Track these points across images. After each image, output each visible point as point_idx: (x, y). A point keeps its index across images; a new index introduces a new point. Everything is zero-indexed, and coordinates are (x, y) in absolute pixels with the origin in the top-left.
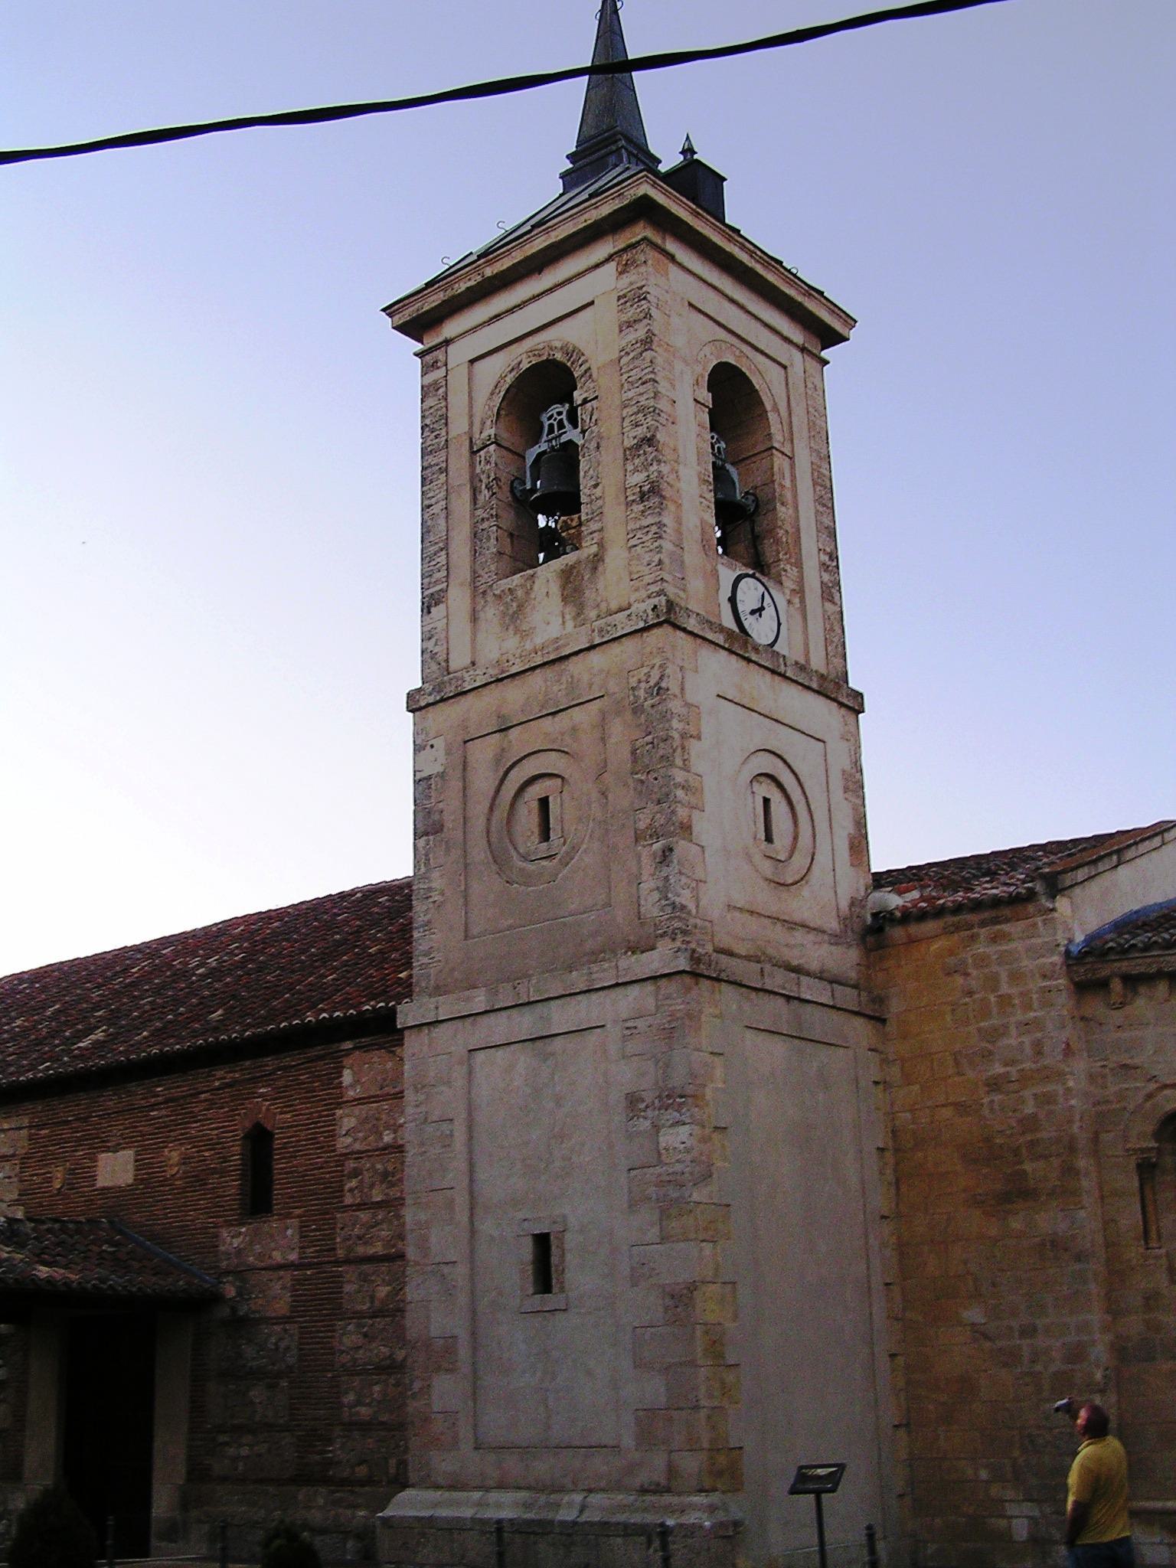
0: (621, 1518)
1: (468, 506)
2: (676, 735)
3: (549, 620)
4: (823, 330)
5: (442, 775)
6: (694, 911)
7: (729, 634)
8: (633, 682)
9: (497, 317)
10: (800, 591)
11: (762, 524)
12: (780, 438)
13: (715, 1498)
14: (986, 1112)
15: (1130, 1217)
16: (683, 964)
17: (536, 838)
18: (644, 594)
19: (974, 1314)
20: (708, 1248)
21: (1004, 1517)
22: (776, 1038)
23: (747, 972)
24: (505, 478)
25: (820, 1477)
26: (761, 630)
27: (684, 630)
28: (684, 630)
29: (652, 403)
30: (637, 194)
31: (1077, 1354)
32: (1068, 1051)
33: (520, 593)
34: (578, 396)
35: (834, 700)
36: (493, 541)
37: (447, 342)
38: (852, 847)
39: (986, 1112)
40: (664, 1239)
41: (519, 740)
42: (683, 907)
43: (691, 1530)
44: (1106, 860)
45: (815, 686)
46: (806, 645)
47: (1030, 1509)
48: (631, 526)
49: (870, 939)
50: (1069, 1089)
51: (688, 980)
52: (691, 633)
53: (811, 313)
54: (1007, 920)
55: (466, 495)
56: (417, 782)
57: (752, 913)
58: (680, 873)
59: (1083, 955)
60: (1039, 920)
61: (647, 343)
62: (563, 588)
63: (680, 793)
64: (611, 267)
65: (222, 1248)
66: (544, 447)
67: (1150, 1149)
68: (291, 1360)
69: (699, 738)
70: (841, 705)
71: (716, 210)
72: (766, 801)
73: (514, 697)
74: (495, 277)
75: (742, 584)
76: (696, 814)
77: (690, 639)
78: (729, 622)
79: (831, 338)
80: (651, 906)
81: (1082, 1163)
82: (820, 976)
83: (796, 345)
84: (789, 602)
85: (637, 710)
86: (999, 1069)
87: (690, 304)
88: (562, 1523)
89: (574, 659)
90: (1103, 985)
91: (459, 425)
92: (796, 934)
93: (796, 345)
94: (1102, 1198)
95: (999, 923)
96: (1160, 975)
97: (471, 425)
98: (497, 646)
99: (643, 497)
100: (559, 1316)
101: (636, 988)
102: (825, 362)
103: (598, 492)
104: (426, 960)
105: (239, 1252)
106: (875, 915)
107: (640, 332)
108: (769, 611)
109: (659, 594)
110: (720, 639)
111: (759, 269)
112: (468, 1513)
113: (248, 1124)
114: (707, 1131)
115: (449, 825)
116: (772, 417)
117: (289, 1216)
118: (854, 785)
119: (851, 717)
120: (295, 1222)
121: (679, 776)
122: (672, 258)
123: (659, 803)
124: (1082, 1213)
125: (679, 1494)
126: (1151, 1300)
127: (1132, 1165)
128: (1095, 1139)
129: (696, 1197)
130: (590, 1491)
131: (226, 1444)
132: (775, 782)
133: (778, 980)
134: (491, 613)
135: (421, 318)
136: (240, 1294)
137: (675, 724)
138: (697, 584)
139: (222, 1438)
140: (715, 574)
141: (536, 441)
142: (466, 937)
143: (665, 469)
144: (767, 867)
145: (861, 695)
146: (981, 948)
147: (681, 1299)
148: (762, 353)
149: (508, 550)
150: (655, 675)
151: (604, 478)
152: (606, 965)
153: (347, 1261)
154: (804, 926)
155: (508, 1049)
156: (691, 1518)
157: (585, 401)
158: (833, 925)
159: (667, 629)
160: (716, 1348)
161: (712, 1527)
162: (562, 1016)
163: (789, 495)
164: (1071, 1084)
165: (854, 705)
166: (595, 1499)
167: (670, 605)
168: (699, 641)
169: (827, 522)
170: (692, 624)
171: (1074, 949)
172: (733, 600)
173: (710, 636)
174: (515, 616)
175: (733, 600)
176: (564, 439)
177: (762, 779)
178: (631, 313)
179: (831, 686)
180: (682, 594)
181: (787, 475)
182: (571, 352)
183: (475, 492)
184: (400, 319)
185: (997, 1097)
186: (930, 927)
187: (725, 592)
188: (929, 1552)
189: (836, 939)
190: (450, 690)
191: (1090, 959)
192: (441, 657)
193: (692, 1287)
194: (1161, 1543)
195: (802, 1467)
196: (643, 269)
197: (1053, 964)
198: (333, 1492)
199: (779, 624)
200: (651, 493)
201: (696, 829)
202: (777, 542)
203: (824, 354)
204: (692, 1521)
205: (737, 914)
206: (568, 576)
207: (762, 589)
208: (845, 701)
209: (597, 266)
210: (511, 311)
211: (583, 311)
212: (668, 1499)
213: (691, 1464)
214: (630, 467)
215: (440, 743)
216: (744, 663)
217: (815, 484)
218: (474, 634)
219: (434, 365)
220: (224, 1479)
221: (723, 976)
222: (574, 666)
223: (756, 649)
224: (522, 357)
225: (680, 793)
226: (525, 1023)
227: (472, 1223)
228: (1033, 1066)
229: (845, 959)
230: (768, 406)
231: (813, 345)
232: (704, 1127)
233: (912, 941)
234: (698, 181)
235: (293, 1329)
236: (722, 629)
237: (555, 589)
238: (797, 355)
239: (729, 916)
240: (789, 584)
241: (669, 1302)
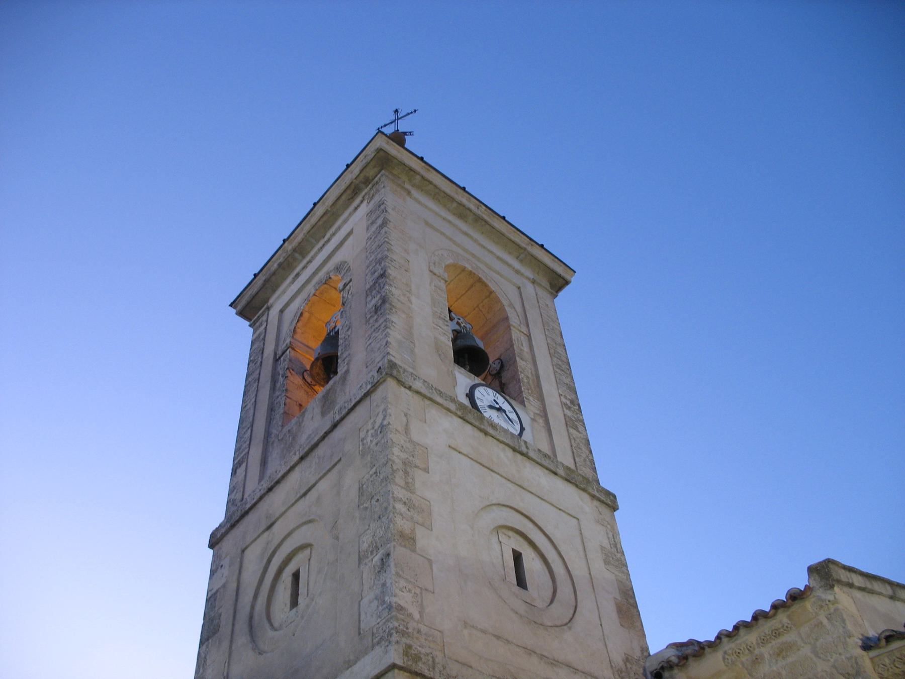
6: (417, 616)
7: (461, 406)
38: (620, 610)
42: (400, 608)
52: (418, 392)
54: (787, 629)
63: (399, 506)
64: (365, 202)
69: (426, 470)
70: (593, 497)
72: (517, 557)
79: (558, 283)
84: (533, 420)
110: (453, 407)
119: (606, 511)
121: (400, 493)
137: (396, 450)
145: (614, 496)
154: (569, 666)
168: (428, 402)
170: (418, 385)
179: (580, 479)
184: (239, 307)
216: (482, 435)
225: (399, 506)
230: (505, 303)
236: (453, 400)
239: (466, 632)
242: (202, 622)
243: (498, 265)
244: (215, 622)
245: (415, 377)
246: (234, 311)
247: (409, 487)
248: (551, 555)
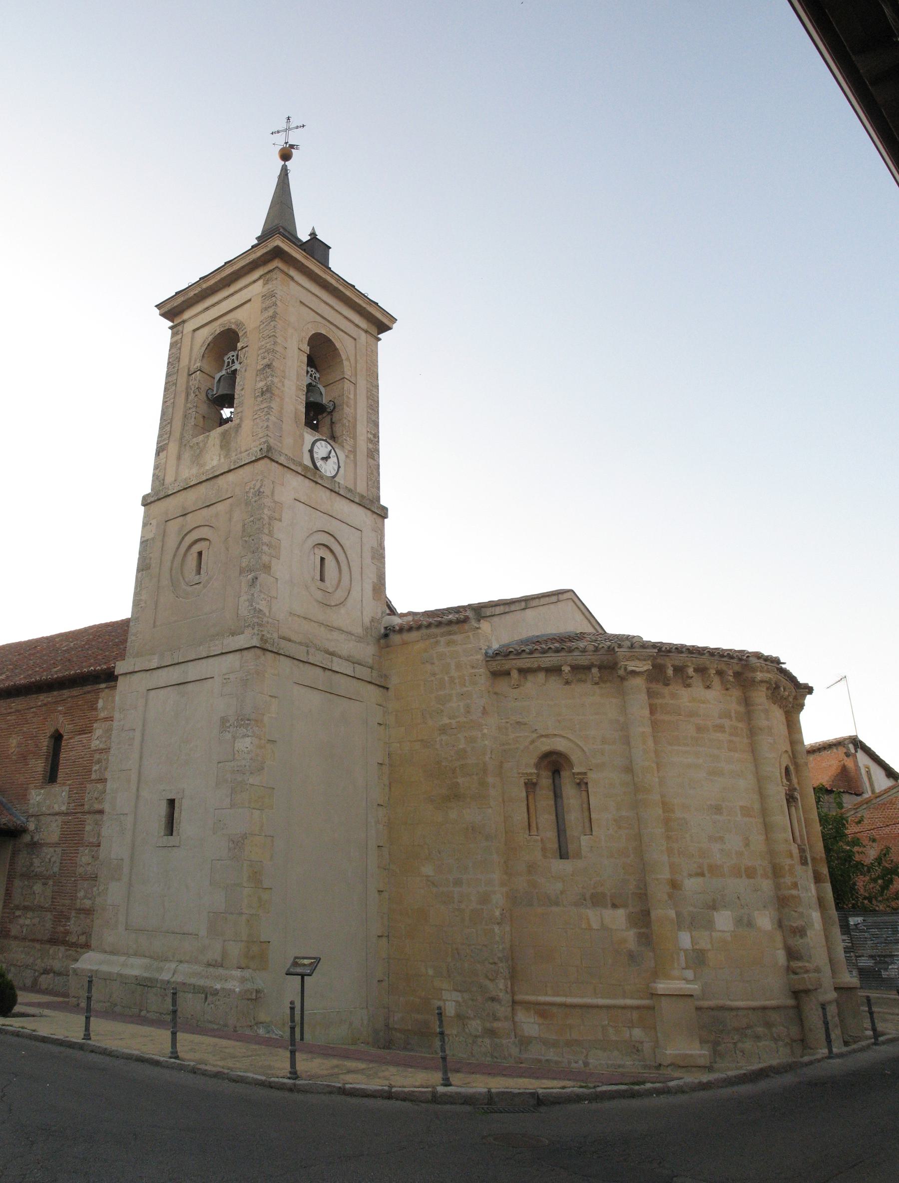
0: (193, 981)
1: (183, 401)
2: (266, 518)
3: (214, 460)
4: (380, 323)
5: (153, 539)
7: (306, 467)
8: (247, 488)
9: (207, 309)
10: (354, 451)
11: (336, 416)
12: (349, 373)
13: (247, 973)
14: (438, 746)
15: (520, 815)
16: (255, 642)
17: (194, 573)
18: (258, 443)
19: (428, 870)
20: (257, 813)
21: (440, 999)
22: (315, 692)
23: (292, 649)
24: (204, 388)
25: (305, 965)
26: (328, 469)
27: (277, 462)
28: (277, 462)
29: (272, 347)
30: (286, 251)
31: (485, 899)
32: (485, 712)
33: (201, 445)
34: (239, 345)
35: (369, 509)
36: (193, 419)
37: (184, 322)
39: (438, 746)
40: (232, 806)
41: (191, 521)
43: (229, 993)
44: (517, 604)
45: (357, 500)
46: (355, 479)
47: (456, 996)
48: (256, 408)
49: (382, 641)
50: (484, 735)
51: (258, 652)
53: (370, 313)
54: (455, 633)
55: (183, 396)
56: (142, 543)
57: (305, 618)
58: (261, 591)
59: (497, 654)
60: (470, 634)
61: (273, 317)
62: (221, 442)
63: (265, 548)
64: (260, 282)
65: (31, 801)
66: (224, 372)
67: (531, 774)
68: (56, 869)
69: (280, 520)
70: (374, 512)
71: (324, 261)
73: (190, 498)
74: (207, 288)
75: (318, 444)
76: (274, 561)
77: (280, 467)
78: (307, 461)
79: (383, 328)
80: (244, 611)
81: (490, 780)
82: (348, 659)
83: (363, 330)
84: (347, 456)
85: (247, 504)
86: (446, 721)
87: (301, 302)
88: (162, 981)
89: (221, 477)
90: (507, 673)
91: (184, 362)
92: (333, 633)
93: (363, 330)
94: (504, 801)
95: (450, 634)
96: (539, 669)
97: (190, 362)
98: (189, 473)
99: (263, 394)
100: (175, 849)
101: (231, 656)
102: (380, 339)
103: (243, 392)
104: (134, 638)
105: (39, 804)
106: (386, 628)
107: (270, 312)
108: (333, 459)
109: (265, 443)
110: (299, 470)
111: (341, 288)
112: (115, 969)
113: (52, 730)
114: (263, 742)
115: (153, 565)
116: (346, 363)
117: (64, 784)
118: (379, 555)
119: (379, 520)
120: (67, 788)
121: (266, 539)
122: (292, 278)
123: (253, 552)
124: (490, 810)
125: (227, 968)
126: (531, 868)
127: (522, 781)
128: (501, 766)
129: (251, 781)
130: (181, 962)
131: (20, 916)
132: (327, 550)
133: (317, 658)
134: (187, 455)
135: (173, 310)
136: (36, 829)
137: (266, 511)
138: (288, 441)
139: (18, 913)
140: (302, 437)
141: (221, 370)
142: (154, 627)
143: (276, 380)
144: (319, 595)
145: (387, 509)
146: (441, 649)
147: (238, 843)
148: (342, 331)
149: (201, 424)
150: (258, 485)
151: (247, 385)
152: (217, 642)
153: (89, 813)
155: (166, 690)
156: (229, 985)
157: (243, 348)
158: (359, 631)
159: (267, 461)
160: (256, 877)
161: (240, 992)
162: (193, 671)
163: (352, 402)
164: (485, 731)
165: (382, 513)
166: (183, 967)
167: (269, 448)
168: (286, 469)
169: (374, 418)
170: (282, 460)
171: (490, 652)
172: (311, 451)
173: (293, 467)
174: (198, 458)
177: (321, 547)
178: (268, 303)
179: (368, 502)
180: (279, 444)
181: (352, 392)
182: (240, 324)
183: (187, 395)
185: (444, 738)
186: (414, 635)
187: (307, 446)
188: (396, 1019)
189: (360, 639)
190: (162, 495)
191: (499, 658)
192: (161, 477)
193: (244, 837)
194: (534, 1023)
195: (296, 958)
196: (275, 282)
197: (478, 660)
198: (67, 950)
199: (339, 467)
200: (267, 392)
201: (272, 570)
202: (343, 425)
203: (380, 336)
204: (229, 987)
205: (296, 618)
206: (224, 435)
207: (329, 448)
208: (376, 511)
210: (213, 305)
211: (245, 305)
212: (221, 971)
213: (235, 950)
215: (154, 522)
216: (313, 484)
217: (368, 398)
218: (178, 466)
220: (16, 938)
221: (281, 652)
222: (221, 481)
223: (322, 477)
224: (217, 328)
225: (265, 548)
226: (174, 675)
227: (138, 790)
228: (465, 720)
229: (367, 651)
230: (344, 357)
231: (373, 330)
232: (260, 739)
233: (405, 643)
234: (317, 248)
235: (59, 850)
236: (301, 464)
237: (218, 442)
238: (363, 335)
239: (290, 619)
240: (348, 447)
241: (231, 845)
242: (138, 556)
243: (344, 324)
244: (148, 561)
245: (280, 453)
246: (158, 311)
247: (270, 534)
248: (341, 557)
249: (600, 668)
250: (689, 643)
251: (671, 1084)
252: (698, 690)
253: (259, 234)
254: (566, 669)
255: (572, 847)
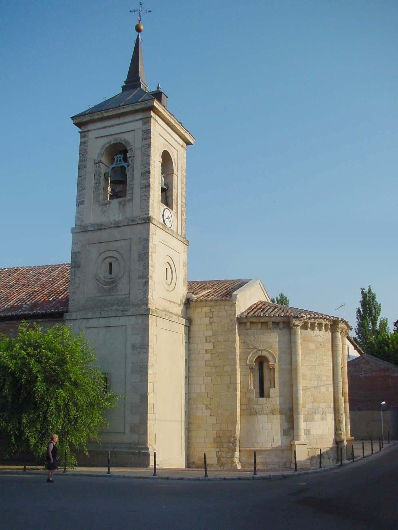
37: (89, 131)
64: (141, 122)
103: (132, 183)
116: (174, 164)
135: (82, 121)
144: (166, 286)
157: (130, 157)
158: (179, 302)
172: (163, 216)
175: (163, 216)
176: (121, 165)
182: (127, 142)
209: (137, 120)
214: (142, 178)
219: (85, 136)
224: (111, 140)
230: (173, 162)
249: (283, 322)
250: (77, 157)
251: (309, 471)
252: (317, 331)
253: (126, 80)
254: (270, 323)
255: (266, 393)
